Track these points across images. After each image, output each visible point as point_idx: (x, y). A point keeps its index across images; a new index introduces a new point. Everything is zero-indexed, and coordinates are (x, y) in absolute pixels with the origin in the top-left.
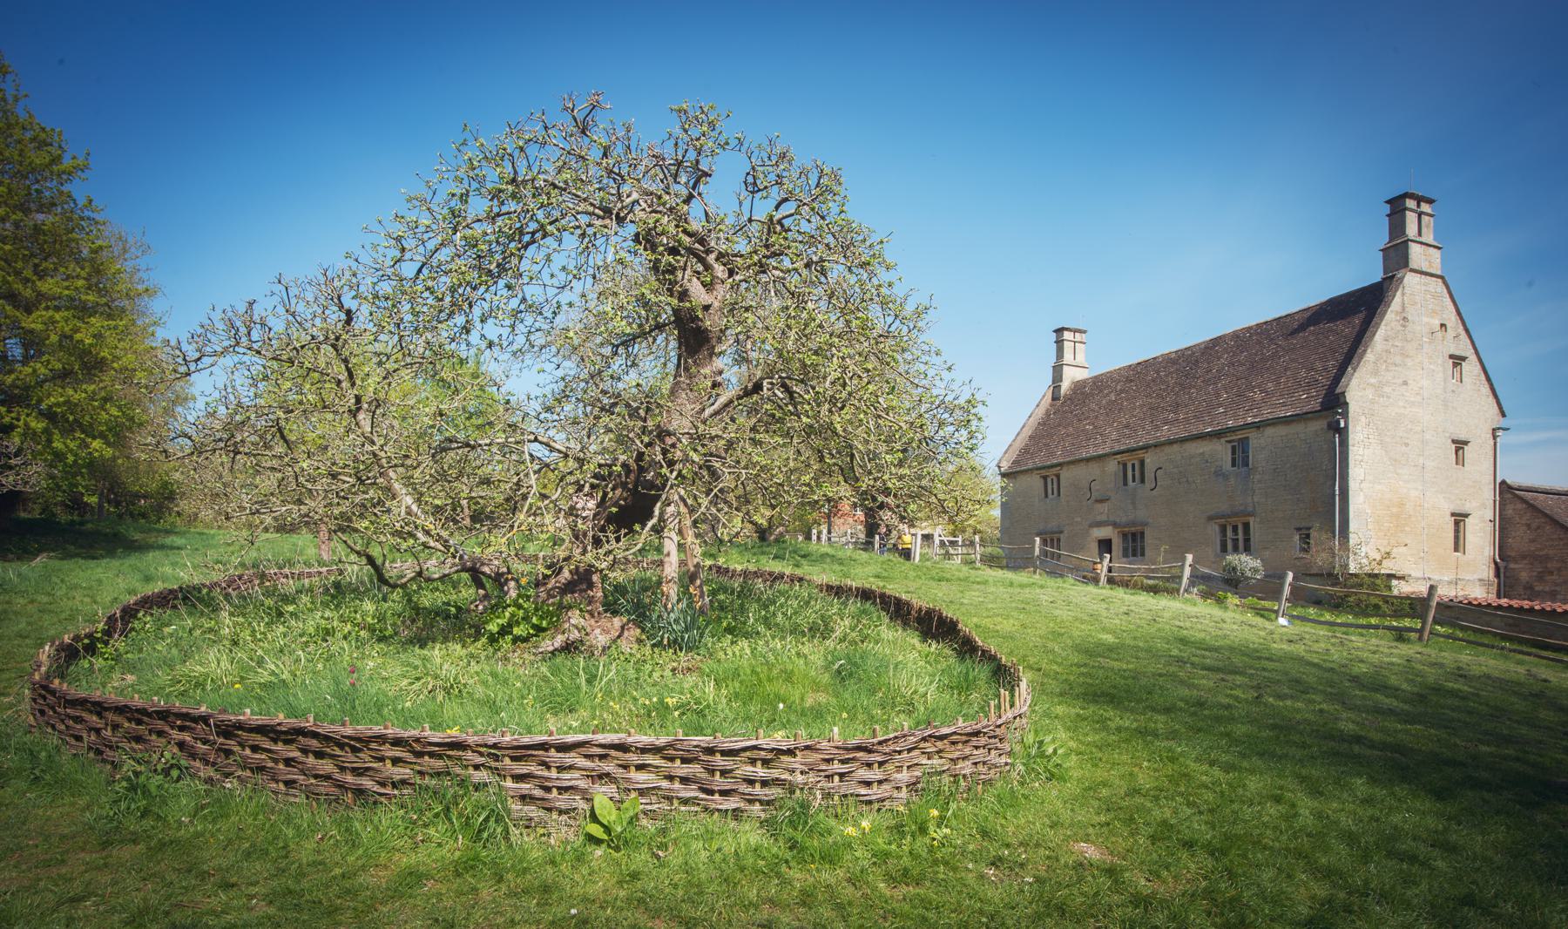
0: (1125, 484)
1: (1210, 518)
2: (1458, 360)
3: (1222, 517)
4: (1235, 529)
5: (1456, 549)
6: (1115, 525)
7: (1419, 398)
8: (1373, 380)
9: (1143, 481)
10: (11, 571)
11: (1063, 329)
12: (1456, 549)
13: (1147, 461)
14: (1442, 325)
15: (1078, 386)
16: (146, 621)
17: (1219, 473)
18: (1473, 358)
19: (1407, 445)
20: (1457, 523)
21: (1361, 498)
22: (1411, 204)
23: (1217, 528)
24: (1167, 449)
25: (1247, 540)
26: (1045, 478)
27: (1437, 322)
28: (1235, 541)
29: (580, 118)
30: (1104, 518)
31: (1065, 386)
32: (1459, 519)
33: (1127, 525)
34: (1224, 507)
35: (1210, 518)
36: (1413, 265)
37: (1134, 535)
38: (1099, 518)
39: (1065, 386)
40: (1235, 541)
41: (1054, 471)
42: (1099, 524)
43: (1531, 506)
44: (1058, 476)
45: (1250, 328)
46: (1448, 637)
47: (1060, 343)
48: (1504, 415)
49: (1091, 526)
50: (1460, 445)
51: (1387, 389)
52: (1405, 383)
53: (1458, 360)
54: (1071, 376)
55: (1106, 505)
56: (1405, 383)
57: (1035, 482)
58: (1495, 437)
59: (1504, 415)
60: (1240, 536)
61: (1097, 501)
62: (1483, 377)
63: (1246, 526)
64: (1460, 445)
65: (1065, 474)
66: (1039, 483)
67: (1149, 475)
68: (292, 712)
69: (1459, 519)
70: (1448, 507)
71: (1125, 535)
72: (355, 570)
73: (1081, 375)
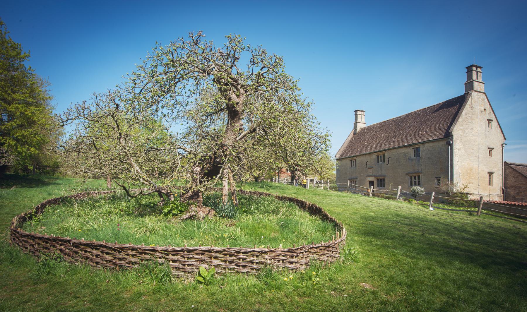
0: (378, 162)
1: (407, 174)
2: (490, 121)
3: (411, 174)
4: (415, 178)
5: (489, 184)
6: (375, 176)
7: (477, 134)
8: (461, 128)
9: (384, 161)
11: (357, 111)
12: (489, 184)
13: (386, 155)
14: (485, 109)
15: (362, 130)
16: (49, 209)
17: (410, 159)
18: (495, 120)
19: (473, 149)
20: (490, 176)
21: (458, 167)
22: (474, 68)
23: (409, 177)
24: (392, 151)
25: (419, 181)
26: (351, 161)
27: (483, 108)
28: (415, 182)
29: (195, 39)
30: (371, 174)
31: (358, 130)
32: (490, 174)
33: (379, 176)
34: (411, 170)
35: (407, 174)
36: (475, 89)
37: (381, 180)
38: (369, 174)
39: (358, 130)
40: (415, 182)
41: (354, 158)
42: (369, 176)
43: (515, 170)
44: (356, 160)
45: (420, 110)
46: (487, 214)
47: (356, 115)
48: (505, 139)
49: (367, 177)
50: (491, 149)
51: (466, 131)
52: (472, 129)
53: (490, 121)
54: (360, 126)
55: (372, 169)
56: (472, 129)
57: (348, 162)
58: (502, 147)
59: (505, 139)
60: (417, 180)
61: (369, 168)
62: (498, 127)
63: (419, 177)
64: (491, 149)
65: (358, 159)
66: (349, 162)
67: (386, 159)
68: (98, 239)
69: (490, 174)
70: (487, 170)
71: (378, 180)
72: (119, 191)
73: (363, 126)
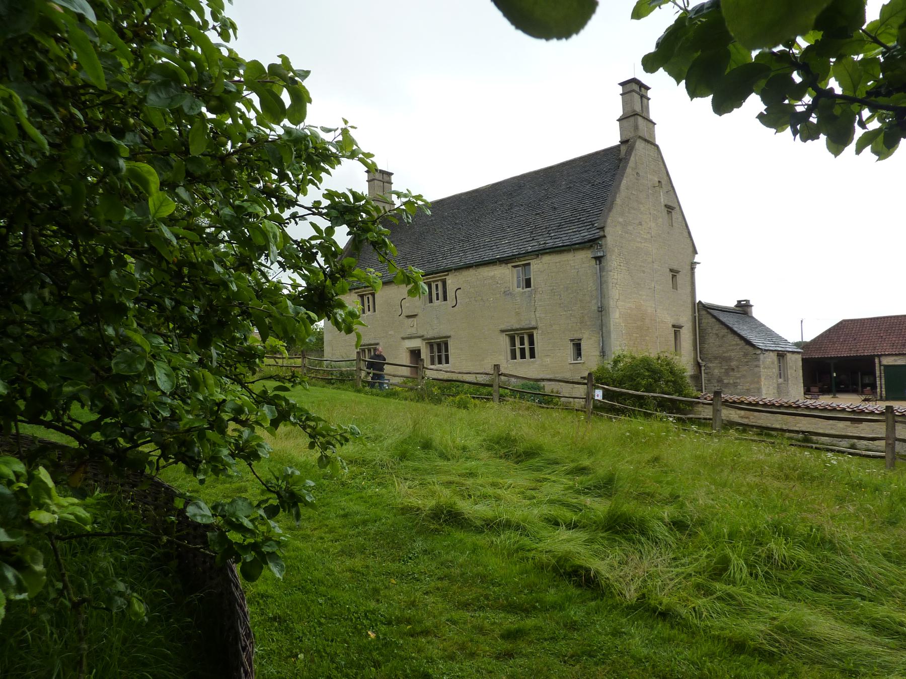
0: (431, 301)
1: (502, 331)
7: (649, 236)
8: (621, 220)
9: (445, 299)
10: (261, 648)
13: (449, 282)
16: (750, 435)
17: (508, 293)
18: (678, 208)
19: (644, 272)
20: (675, 332)
21: (617, 315)
25: (532, 351)
26: (362, 296)
27: (657, 180)
28: (523, 351)
32: (677, 328)
36: (611, 137)
37: (439, 345)
40: (523, 351)
41: (439, 277)
49: (403, 339)
51: (630, 228)
52: (640, 224)
56: (640, 224)
60: (527, 346)
61: (408, 317)
63: (531, 337)
69: (677, 328)
70: (670, 321)
71: (431, 346)
72: (195, 246)
